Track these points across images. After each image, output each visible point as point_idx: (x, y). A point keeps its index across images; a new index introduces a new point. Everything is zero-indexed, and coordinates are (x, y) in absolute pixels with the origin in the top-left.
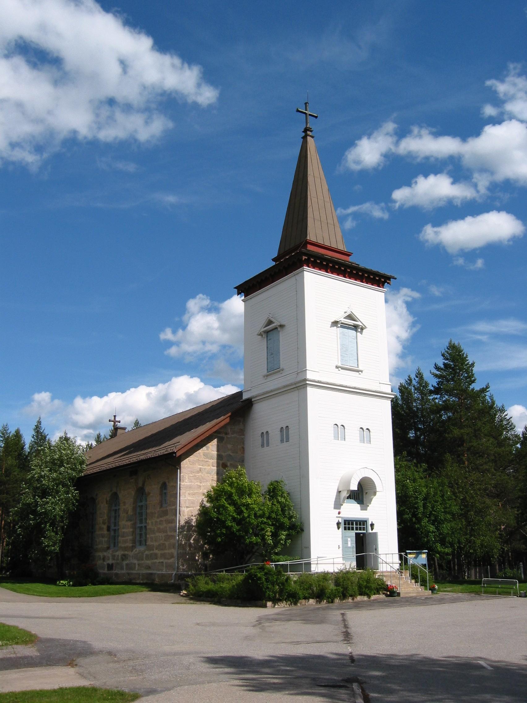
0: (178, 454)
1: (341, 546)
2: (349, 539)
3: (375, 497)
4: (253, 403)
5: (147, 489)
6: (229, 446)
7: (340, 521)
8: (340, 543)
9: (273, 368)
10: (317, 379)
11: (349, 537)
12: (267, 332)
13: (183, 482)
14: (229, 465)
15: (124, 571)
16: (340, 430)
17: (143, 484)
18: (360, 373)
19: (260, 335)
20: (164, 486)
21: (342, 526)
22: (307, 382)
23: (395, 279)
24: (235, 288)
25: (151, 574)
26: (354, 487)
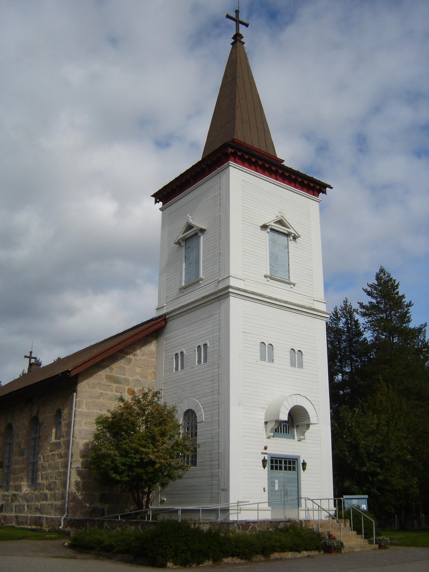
0: (73, 374)
2: (276, 481)
3: (308, 431)
4: (167, 320)
5: (41, 418)
6: (138, 370)
7: (266, 458)
8: (266, 486)
9: (193, 282)
10: (243, 287)
11: (277, 478)
12: (186, 240)
13: (79, 407)
15: (13, 514)
16: (267, 351)
17: (38, 413)
18: (292, 286)
19: (178, 243)
20: (59, 413)
21: (268, 464)
22: (231, 290)
23: (331, 188)
25: (40, 518)
26: (284, 417)
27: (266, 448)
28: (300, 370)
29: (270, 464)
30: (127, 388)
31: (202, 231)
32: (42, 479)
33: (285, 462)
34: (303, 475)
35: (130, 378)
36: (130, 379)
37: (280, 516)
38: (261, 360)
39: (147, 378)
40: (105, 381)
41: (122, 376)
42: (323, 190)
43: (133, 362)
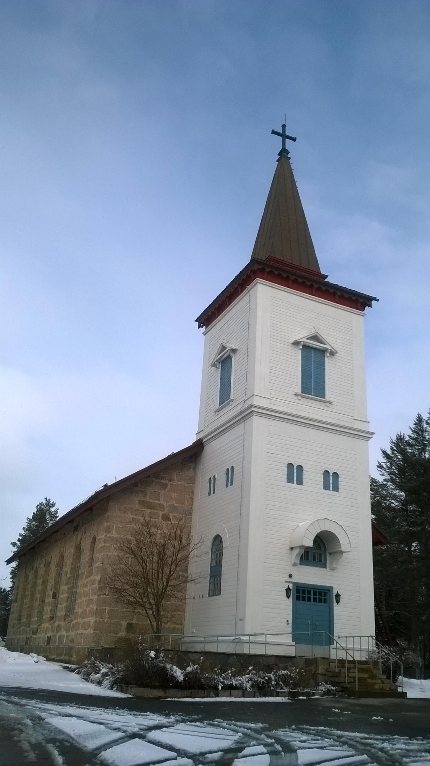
1: (290, 621)
4: (204, 444)
6: (174, 495)
7: (291, 587)
14: (171, 517)
16: (295, 474)
17: (80, 542)
18: (328, 404)
23: (378, 300)
24: (195, 321)
27: (290, 576)
28: (335, 493)
29: (295, 594)
30: (161, 513)
31: (234, 351)
32: (78, 607)
33: (315, 593)
34: (337, 609)
35: (165, 504)
36: (165, 505)
37: (307, 651)
38: (288, 482)
39: (183, 503)
40: (137, 506)
41: (157, 502)
42: (368, 303)
43: (169, 487)
